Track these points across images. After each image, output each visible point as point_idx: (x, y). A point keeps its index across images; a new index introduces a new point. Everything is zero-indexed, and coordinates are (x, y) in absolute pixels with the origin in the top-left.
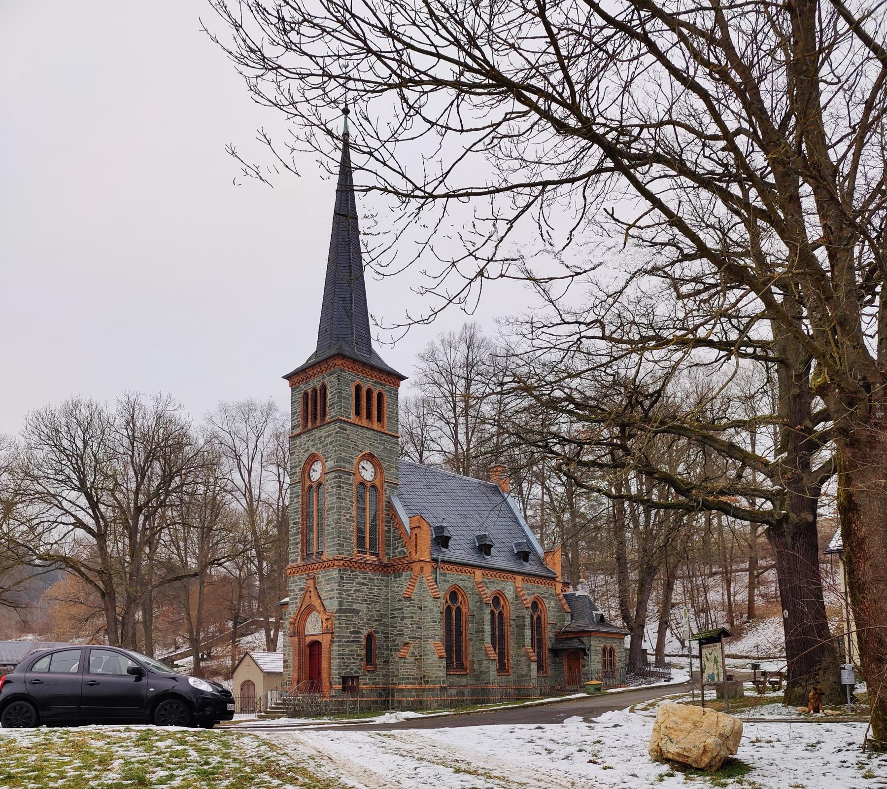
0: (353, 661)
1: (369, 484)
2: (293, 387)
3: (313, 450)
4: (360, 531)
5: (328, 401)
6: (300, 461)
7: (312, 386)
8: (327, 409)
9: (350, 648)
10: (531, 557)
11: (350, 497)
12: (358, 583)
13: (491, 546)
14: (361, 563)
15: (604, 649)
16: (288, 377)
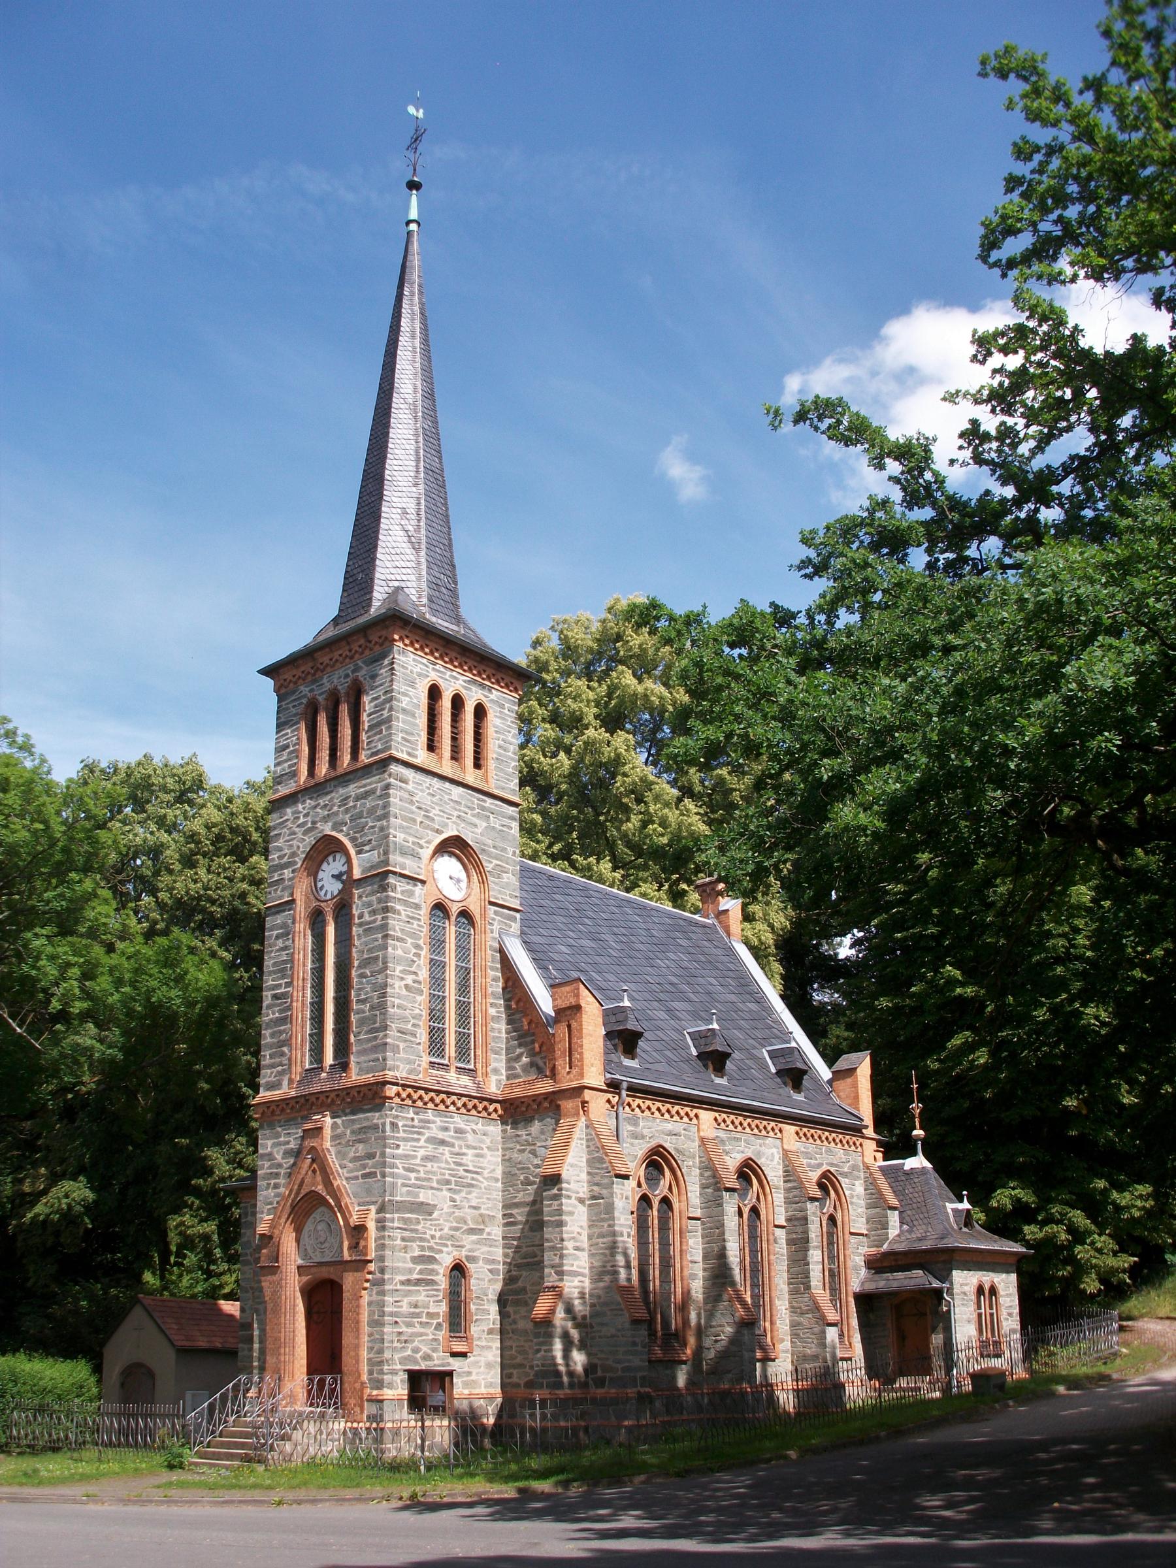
1: (454, 909)
2: (282, 694)
3: (328, 829)
4: (436, 1015)
5: (365, 717)
7: (327, 686)
8: (364, 736)
9: (413, 1299)
11: (413, 935)
12: (431, 1140)
15: (980, 1290)
16: (268, 672)
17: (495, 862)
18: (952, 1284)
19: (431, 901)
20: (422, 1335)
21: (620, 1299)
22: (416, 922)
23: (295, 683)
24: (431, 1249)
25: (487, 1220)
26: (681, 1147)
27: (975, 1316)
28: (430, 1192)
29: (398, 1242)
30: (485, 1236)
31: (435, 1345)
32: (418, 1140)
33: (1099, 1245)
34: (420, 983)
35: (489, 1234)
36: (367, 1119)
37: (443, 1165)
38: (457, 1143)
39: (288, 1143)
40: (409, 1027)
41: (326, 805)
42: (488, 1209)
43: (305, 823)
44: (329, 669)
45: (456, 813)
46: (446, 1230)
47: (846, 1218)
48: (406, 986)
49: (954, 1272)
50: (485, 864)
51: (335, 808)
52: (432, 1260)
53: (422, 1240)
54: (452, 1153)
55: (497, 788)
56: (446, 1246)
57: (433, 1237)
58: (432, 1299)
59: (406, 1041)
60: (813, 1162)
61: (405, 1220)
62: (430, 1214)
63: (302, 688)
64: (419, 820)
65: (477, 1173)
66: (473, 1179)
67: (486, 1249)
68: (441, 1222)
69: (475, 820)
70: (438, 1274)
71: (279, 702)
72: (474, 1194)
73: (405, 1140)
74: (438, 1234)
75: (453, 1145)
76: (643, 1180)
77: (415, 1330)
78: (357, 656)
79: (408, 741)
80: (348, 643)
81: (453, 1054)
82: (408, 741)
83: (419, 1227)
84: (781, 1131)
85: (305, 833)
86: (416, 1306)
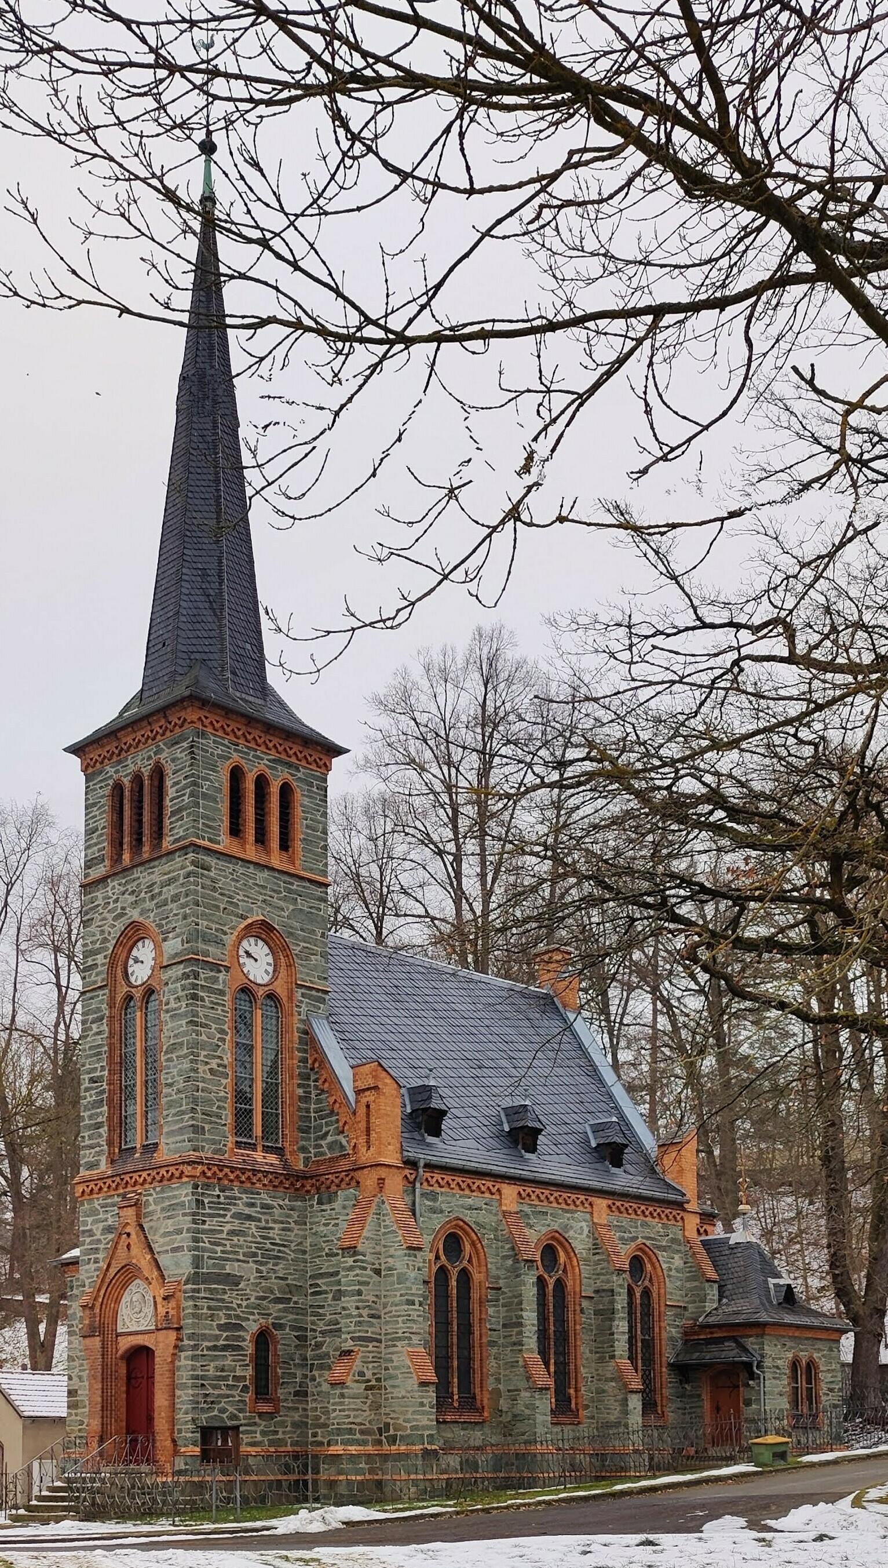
0: (225, 1391)
1: (261, 992)
2: (90, 772)
3: (135, 915)
4: (242, 1097)
5: (167, 802)
6: (105, 940)
7: (132, 768)
8: (167, 822)
9: (219, 1363)
10: (628, 1155)
11: (217, 1020)
12: (237, 1216)
14: (243, 1171)
16: (77, 750)
17: (302, 944)
19: (237, 985)
20: (228, 1396)
21: (410, 1364)
22: (220, 1008)
23: (102, 763)
24: (237, 1317)
25: (293, 1289)
26: (481, 1220)
28: (236, 1264)
29: (205, 1311)
30: (292, 1305)
31: (241, 1406)
32: (225, 1216)
34: (225, 1067)
35: (296, 1303)
36: (175, 1197)
37: (250, 1239)
38: (263, 1217)
39: (106, 1220)
40: (214, 1109)
41: (133, 892)
42: (294, 1279)
43: (115, 909)
44: (132, 750)
45: (261, 898)
46: (253, 1300)
47: (662, 1291)
48: (211, 1070)
50: (291, 947)
51: (143, 895)
52: (240, 1327)
53: (228, 1308)
54: (258, 1227)
55: (303, 870)
56: (253, 1314)
57: (239, 1306)
58: (238, 1364)
59: (211, 1123)
60: (626, 1235)
61: (211, 1291)
62: (238, 1284)
63: (108, 768)
64: (222, 906)
65: (284, 1246)
66: (279, 1251)
67: (291, 1317)
68: (248, 1291)
69: (282, 903)
70: (244, 1340)
71: (87, 781)
72: (281, 1266)
73: (210, 1215)
74: (244, 1303)
75: (259, 1220)
76: (441, 1252)
77: (222, 1392)
78: (159, 737)
79: (209, 827)
80: (150, 724)
81: (260, 1134)
82: (209, 827)
83: (226, 1297)
84: (591, 1204)
85: (115, 919)
86: (222, 1370)
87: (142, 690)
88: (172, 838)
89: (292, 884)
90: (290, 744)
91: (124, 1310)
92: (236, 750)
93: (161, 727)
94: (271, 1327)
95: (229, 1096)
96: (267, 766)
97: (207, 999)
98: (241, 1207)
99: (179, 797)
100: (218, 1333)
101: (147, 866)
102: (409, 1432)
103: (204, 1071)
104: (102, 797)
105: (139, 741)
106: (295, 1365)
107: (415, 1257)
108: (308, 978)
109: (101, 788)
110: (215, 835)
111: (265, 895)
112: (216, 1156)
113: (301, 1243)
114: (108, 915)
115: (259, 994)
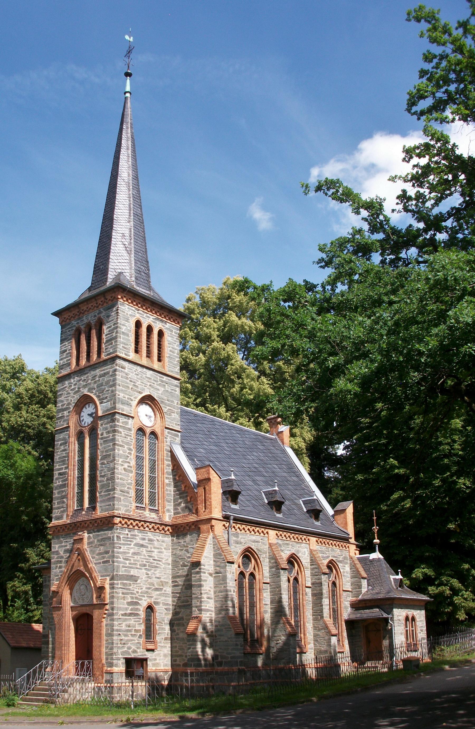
0: (130, 638)
1: (148, 431)
2: (63, 325)
3: (86, 392)
4: (139, 483)
5: (104, 336)
6: (69, 404)
7: (86, 321)
8: (103, 346)
9: (128, 623)
10: (321, 516)
11: (128, 444)
12: (137, 545)
13: (283, 503)
14: (140, 521)
15: (407, 619)
16: (56, 314)
17: (168, 407)
18: (393, 615)
19: (137, 427)
20: (132, 640)
21: (229, 623)
22: (129, 437)
23: (70, 319)
24: (136, 598)
25: (164, 584)
27: (404, 631)
28: (136, 570)
29: (121, 595)
30: (163, 592)
32: (130, 544)
33: (465, 596)
34: (131, 467)
35: (165, 591)
37: (143, 557)
38: (149, 546)
39: (66, 546)
40: (126, 489)
41: (85, 380)
42: (164, 578)
43: (74, 389)
45: (149, 384)
46: (144, 589)
47: (341, 583)
48: (124, 469)
49: (394, 610)
50: (163, 409)
51: (90, 381)
52: (137, 603)
53: (132, 593)
54: (147, 551)
55: (169, 371)
56: (144, 596)
57: (137, 592)
58: (137, 623)
59: (124, 496)
60: (324, 555)
61: (124, 584)
62: (136, 581)
64: (131, 387)
65: (159, 561)
66: (157, 564)
67: (163, 598)
68: (142, 585)
69: (158, 387)
70: (140, 610)
71: (61, 329)
72: (158, 571)
73: (124, 544)
74: (140, 591)
76: (241, 564)
77: (129, 638)
78: (100, 306)
79: (125, 348)
80: (96, 300)
81: (147, 502)
82: (125, 348)
83: (131, 587)
84: (309, 540)
85: (74, 393)
86: (129, 626)
87: (91, 286)
88: (106, 354)
89: (163, 378)
90: (163, 312)
91: (75, 593)
92: (138, 313)
93: (102, 301)
94: (153, 603)
95: (133, 482)
96: (153, 321)
97: (123, 432)
98: (138, 540)
99: (111, 333)
100: (127, 606)
101: (92, 367)
102: (229, 659)
103: (121, 469)
104: (70, 335)
105: (90, 308)
106: (165, 623)
107: (231, 566)
108: (170, 424)
109: (69, 331)
110: (128, 352)
111: (151, 382)
112: (127, 513)
113: (168, 559)
114: (71, 392)
115: (147, 431)
